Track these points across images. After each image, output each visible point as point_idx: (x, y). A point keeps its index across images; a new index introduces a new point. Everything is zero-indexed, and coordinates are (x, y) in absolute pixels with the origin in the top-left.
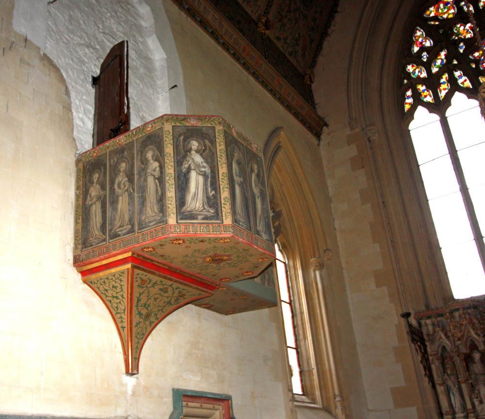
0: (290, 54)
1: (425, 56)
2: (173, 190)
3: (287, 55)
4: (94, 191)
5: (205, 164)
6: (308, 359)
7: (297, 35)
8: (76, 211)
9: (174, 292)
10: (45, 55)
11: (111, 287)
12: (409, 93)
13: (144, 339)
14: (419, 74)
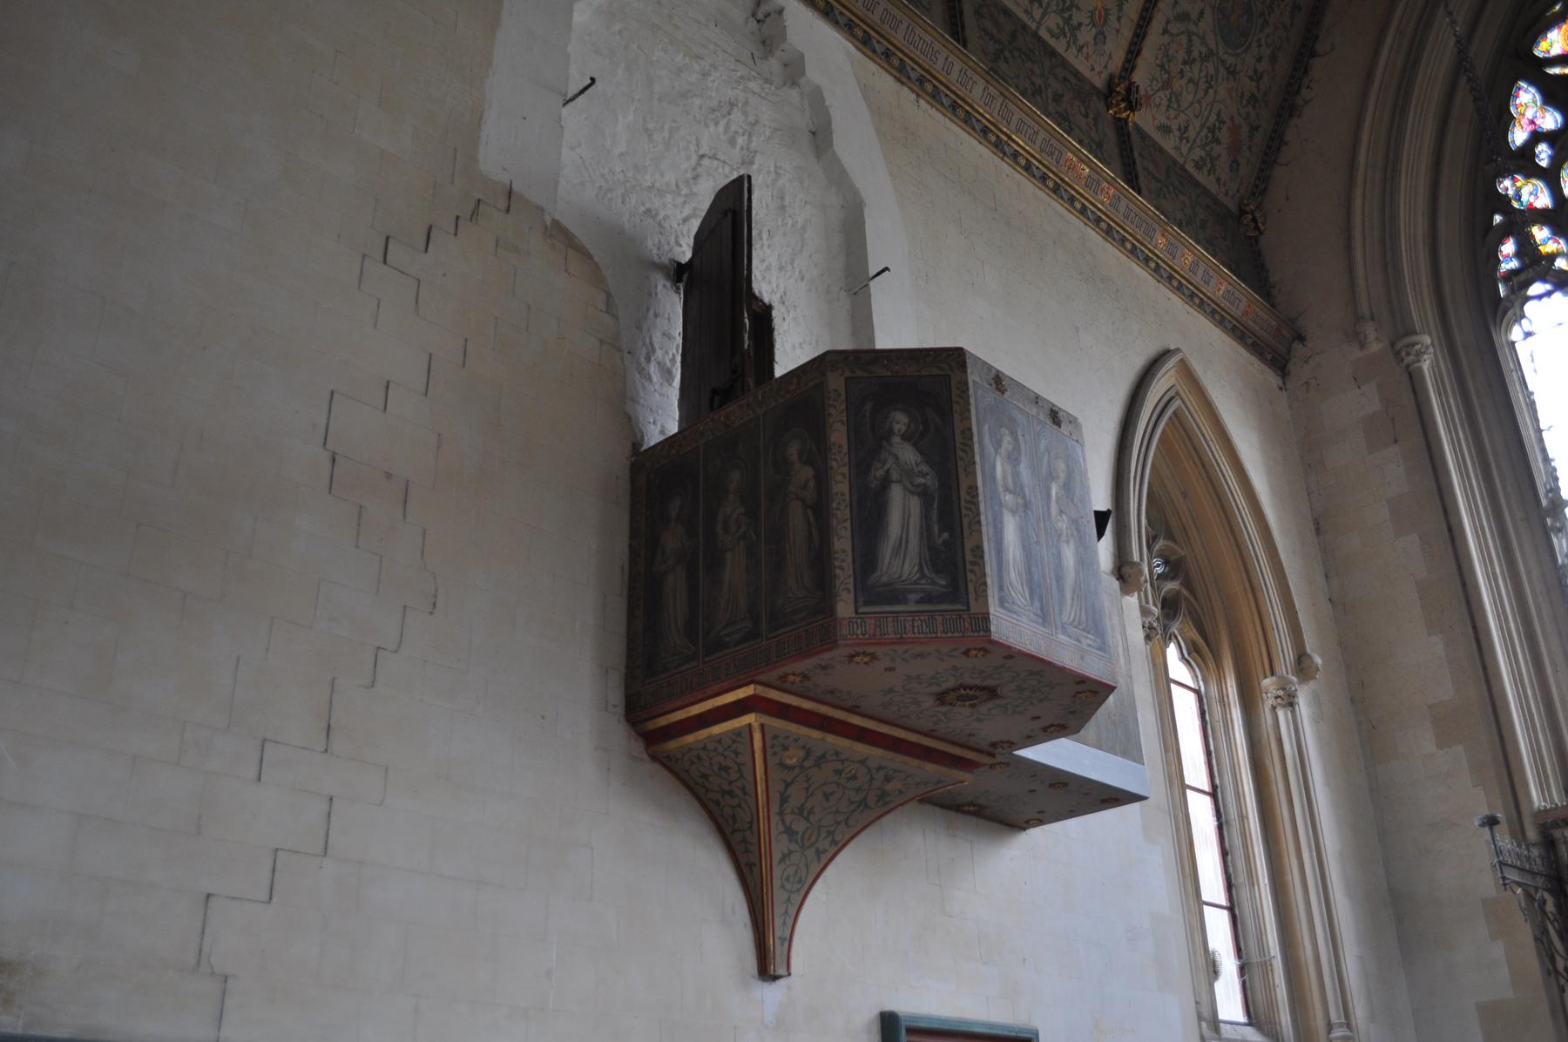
0: (1198, 166)
1: (1543, 154)
2: (848, 534)
3: (1189, 167)
4: (672, 540)
5: (925, 468)
6: (1261, 934)
7: (1213, 118)
8: (631, 588)
9: (872, 779)
10: (556, 223)
11: (716, 767)
12: (1509, 247)
13: (803, 892)
14: (1532, 199)
